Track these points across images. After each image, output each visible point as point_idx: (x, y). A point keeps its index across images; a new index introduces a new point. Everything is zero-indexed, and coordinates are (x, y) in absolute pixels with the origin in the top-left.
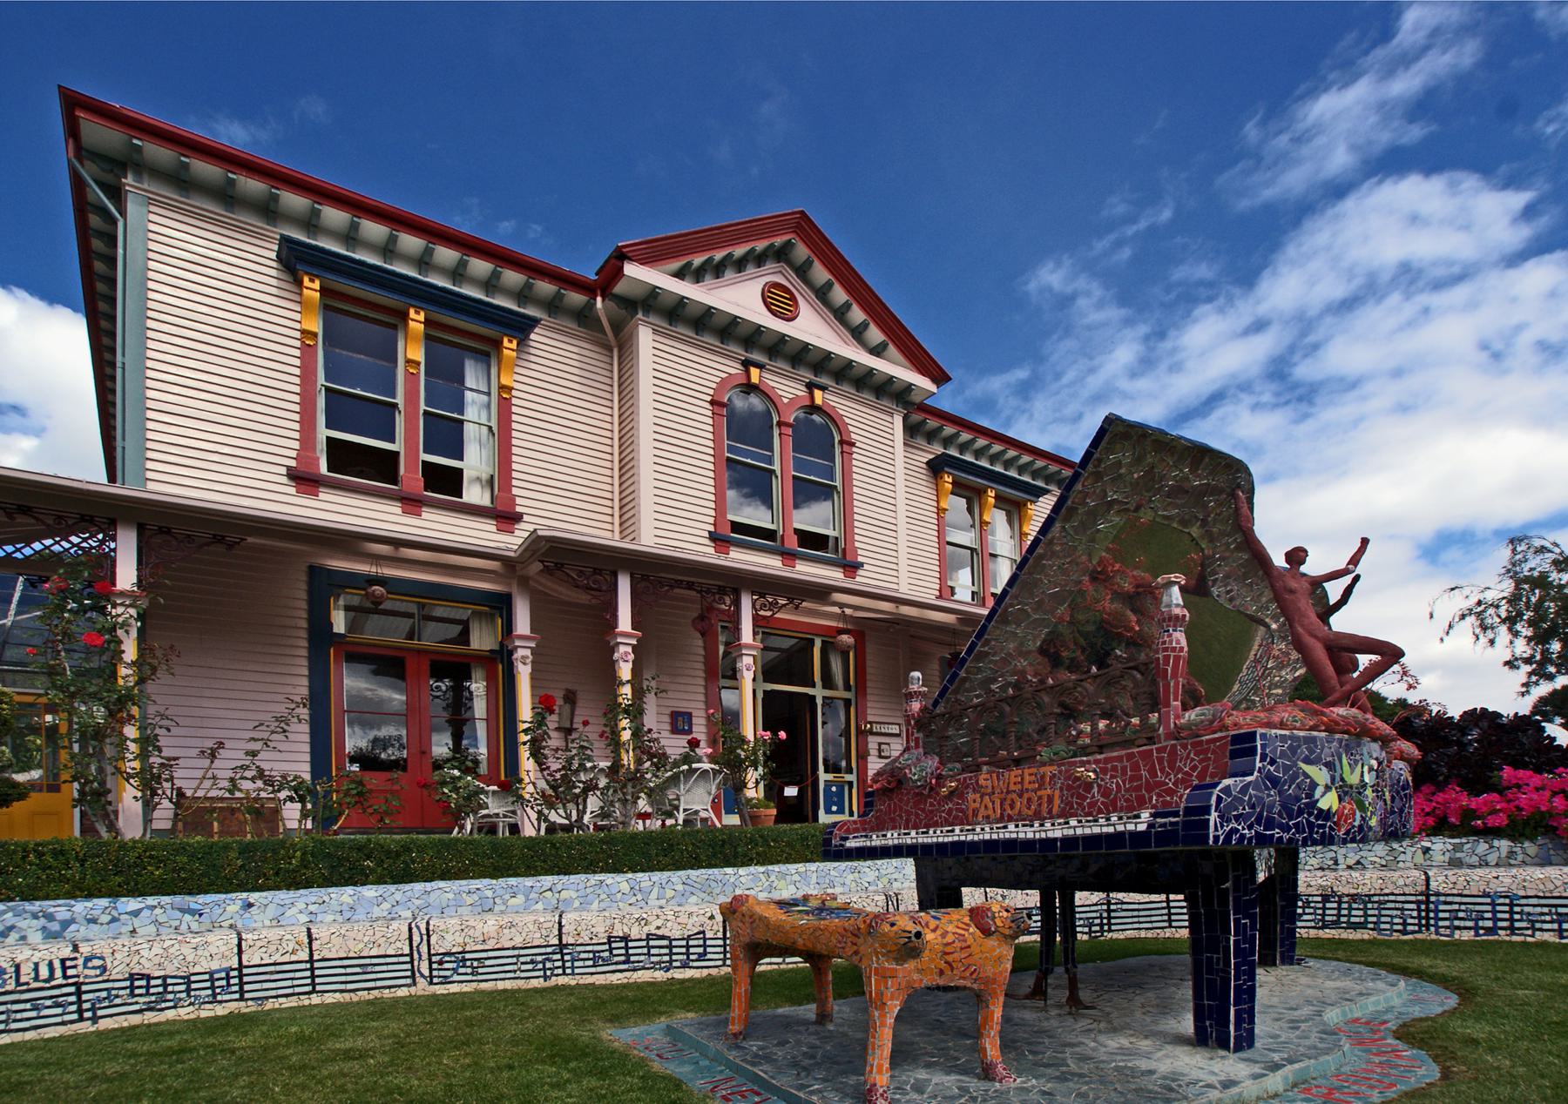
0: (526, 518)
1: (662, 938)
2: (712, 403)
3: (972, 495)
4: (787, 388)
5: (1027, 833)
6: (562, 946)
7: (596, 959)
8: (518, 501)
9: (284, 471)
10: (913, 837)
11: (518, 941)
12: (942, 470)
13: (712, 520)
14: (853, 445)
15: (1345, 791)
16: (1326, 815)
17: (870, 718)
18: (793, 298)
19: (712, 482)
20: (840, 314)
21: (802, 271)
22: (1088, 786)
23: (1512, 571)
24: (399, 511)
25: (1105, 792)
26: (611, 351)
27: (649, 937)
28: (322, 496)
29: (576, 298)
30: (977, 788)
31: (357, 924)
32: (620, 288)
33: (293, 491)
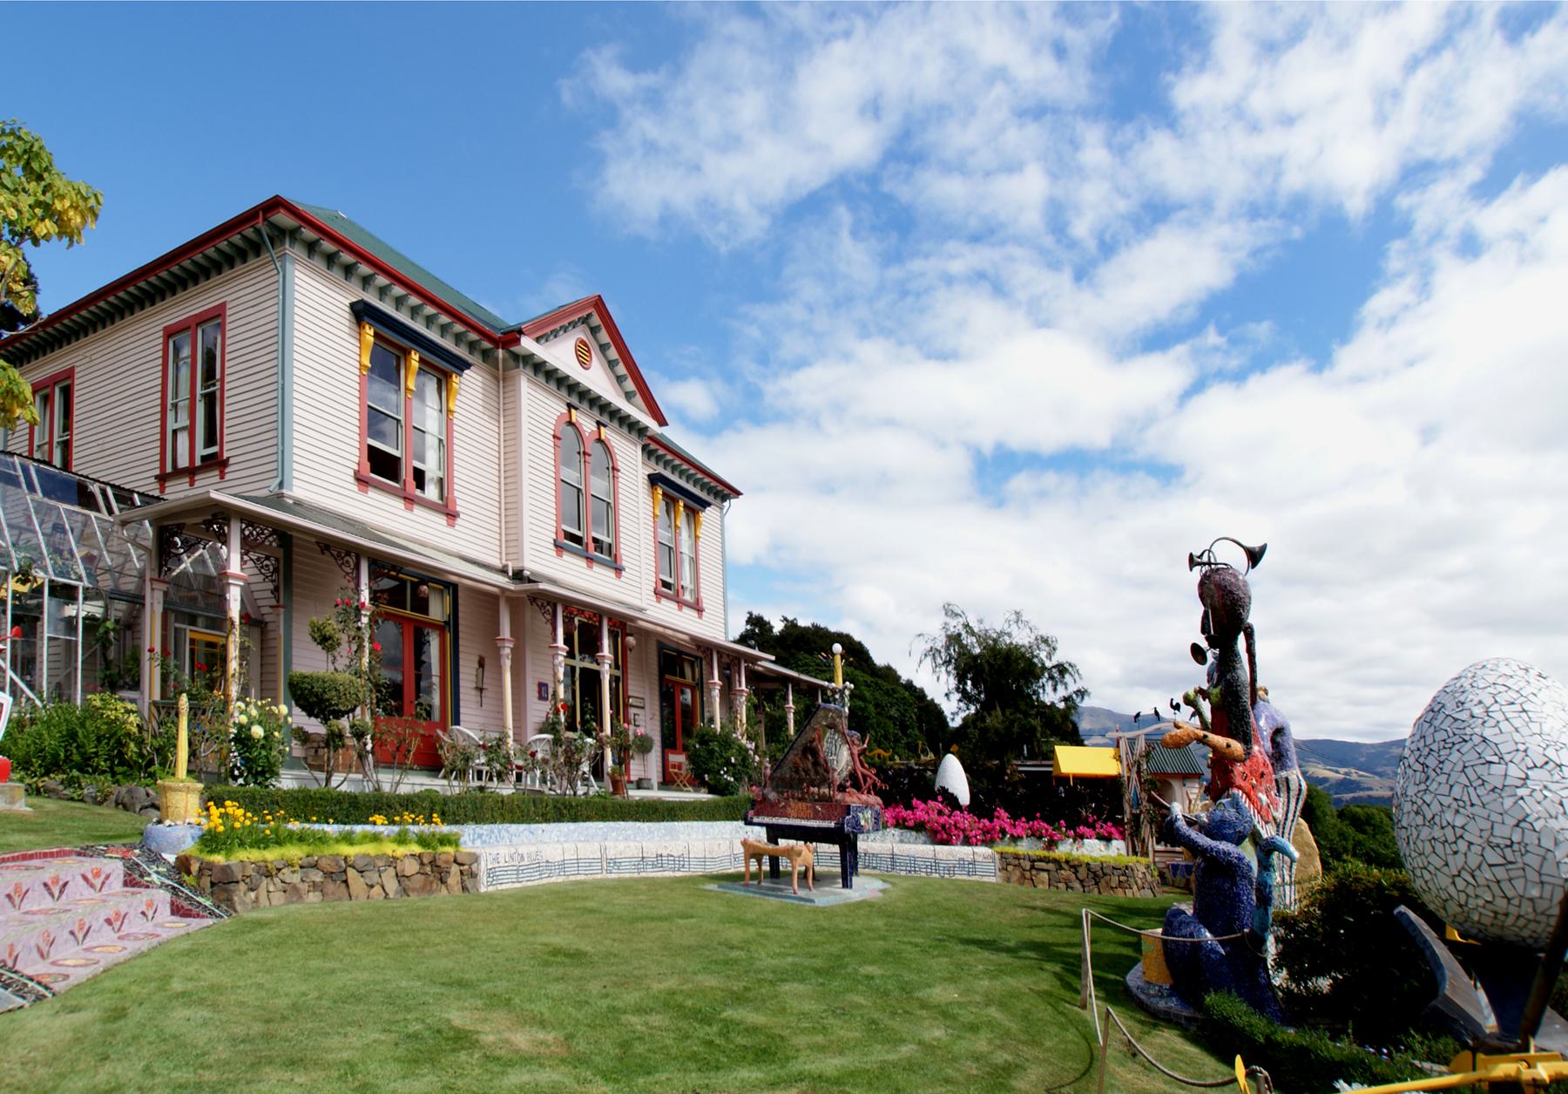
3: (670, 502)
4: (587, 423)
21: (594, 331)
29: (486, 345)
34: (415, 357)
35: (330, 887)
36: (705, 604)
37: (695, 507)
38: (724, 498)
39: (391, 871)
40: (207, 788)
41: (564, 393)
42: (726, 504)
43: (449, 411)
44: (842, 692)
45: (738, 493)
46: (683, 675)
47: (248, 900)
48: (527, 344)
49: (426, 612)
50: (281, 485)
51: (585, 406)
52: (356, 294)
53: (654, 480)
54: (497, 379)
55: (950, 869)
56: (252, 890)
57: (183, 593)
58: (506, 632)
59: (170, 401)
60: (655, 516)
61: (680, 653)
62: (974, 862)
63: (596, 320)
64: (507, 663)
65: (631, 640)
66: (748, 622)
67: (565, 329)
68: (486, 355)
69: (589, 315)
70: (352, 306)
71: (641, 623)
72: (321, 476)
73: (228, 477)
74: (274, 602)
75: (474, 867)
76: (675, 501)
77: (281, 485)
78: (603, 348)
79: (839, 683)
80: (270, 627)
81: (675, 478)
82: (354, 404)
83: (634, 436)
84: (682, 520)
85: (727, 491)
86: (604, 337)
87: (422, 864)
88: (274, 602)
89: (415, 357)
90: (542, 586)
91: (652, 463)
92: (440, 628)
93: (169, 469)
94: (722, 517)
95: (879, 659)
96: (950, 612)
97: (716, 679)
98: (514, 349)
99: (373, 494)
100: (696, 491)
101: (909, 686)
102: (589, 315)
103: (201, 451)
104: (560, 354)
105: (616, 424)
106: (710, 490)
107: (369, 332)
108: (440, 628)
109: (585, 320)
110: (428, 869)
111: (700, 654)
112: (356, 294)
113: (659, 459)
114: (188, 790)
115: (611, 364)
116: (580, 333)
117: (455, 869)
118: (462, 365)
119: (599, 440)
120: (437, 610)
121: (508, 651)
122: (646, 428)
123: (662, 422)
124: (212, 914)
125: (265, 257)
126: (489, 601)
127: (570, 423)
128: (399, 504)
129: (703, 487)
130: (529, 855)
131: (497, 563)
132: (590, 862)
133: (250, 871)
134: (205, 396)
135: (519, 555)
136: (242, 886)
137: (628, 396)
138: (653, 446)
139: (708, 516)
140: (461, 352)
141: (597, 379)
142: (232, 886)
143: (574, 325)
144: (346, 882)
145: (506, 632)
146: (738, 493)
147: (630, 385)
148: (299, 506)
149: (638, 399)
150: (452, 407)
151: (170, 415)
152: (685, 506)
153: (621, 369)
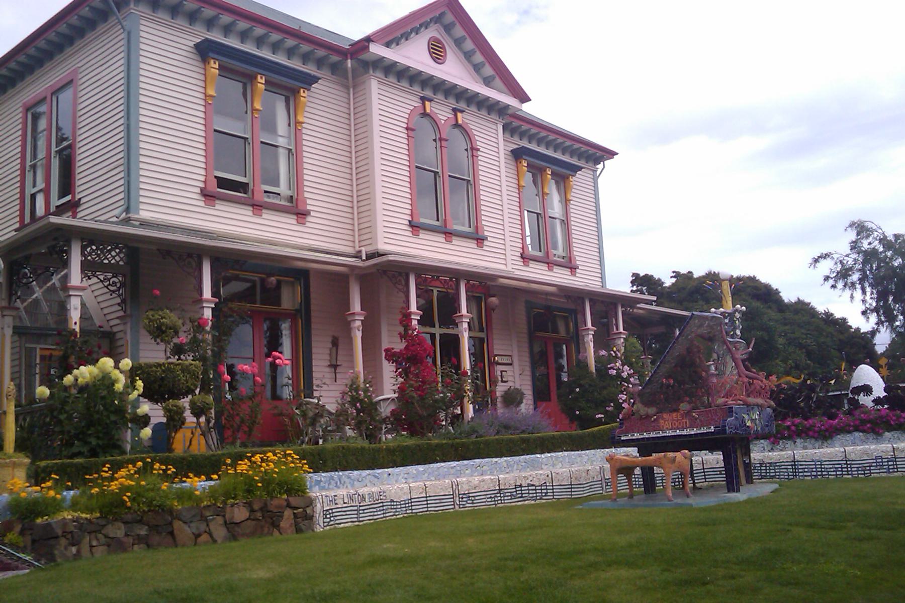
0: (312, 214)
1: (533, 485)
2: (407, 129)
3: (537, 172)
4: (442, 111)
5: (685, 433)
6: (500, 490)
7: (512, 496)
8: (309, 202)
9: (198, 190)
10: (637, 436)
11: (486, 488)
12: (521, 158)
13: (409, 212)
14: (478, 150)
15: (752, 420)
16: (748, 427)
17: (496, 353)
18: (443, 48)
19: (408, 185)
20: (477, 68)
21: (448, 28)
22: (696, 419)
23: (854, 246)
24: (250, 213)
25: (701, 421)
26: (349, 90)
27: (529, 485)
28: (217, 207)
29: (335, 58)
30: (663, 419)
31: (403, 484)
32: (364, 56)
33: (202, 204)
34: (261, 80)
35: (156, 539)
36: (579, 261)
37: (564, 175)
38: (598, 160)
39: (220, 520)
40: (32, 463)
41: (417, 88)
42: (600, 166)
43: (297, 123)
44: (731, 315)
45: (611, 154)
46: (555, 330)
47: (68, 553)
48: (376, 49)
49: (278, 303)
50: (127, 210)
51: (440, 97)
52: (200, 34)
53: (517, 155)
54: (347, 88)
55: (866, 469)
56: (73, 545)
57: (188, 504)
58: (356, 306)
59: (28, 163)
60: (519, 187)
61: (548, 308)
62: (895, 459)
63: (449, 18)
64: (358, 336)
65: (494, 300)
66: (633, 282)
67: (417, 31)
68: (336, 69)
69: (442, 15)
70: (197, 46)
71: (502, 280)
72: (172, 199)
73: (79, 215)
74: (121, 313)
75: (309, 511)
76: (542, 170)
77: (127, 210)
78: (458, 43)
79: (728, 307)
80: (118, 336)
81: (542, 150)
82: (199, 130)
83: (494, 116)
84: (552, 188)
85: (599, 153)
86: (459, 31)
87: (252, 511)
88: (121, 313)
89: (261, 80)
90: (391, 258)
91: (516, 139)
92: (292, 316)
93: (27, 220)
94: (595, 179)
95: (788, 296)
96: (862, 229)
97: (589, 325)
98: (364, 56)
99: (220, 205)
100: (566, 158)
101: (828, 318)
102: (442, 15)
103: (55, 202)
104: (414, 55)
105: (473, 108)
106: (580, 156)
107: (214, 65)
108: (292, 316)
109: (438, 20)
110: (259, 515)
111: (573, 307)
112: (200, 34)
113: (522, 135)
114: (15, 465)
115: (468, 56)
116: (433, 32)
117: (288, 513)
118: (309, 81)
119: (457, 125)
120: (289, 299)
121: (358, 323)
122: (507, 107)
123: (524, 98)
124: (30, 565)
125: (112, 20)
126: (338, 280)
127: (425, 114)
128: (247, 211)
129: (573, 153)
130: (371, 495)
131: (350, 250)
132: (440, 499)
133: (72, 527)
134: (60, 152)
135: (373, 239)
136: (63, 542)
137: (487, 82)
138: (516, 123)
139: (580, 180)
140: (310, 69)
141: (452, 70)
142: (52, 542)
143: (426, 25)
144: (172, 533)
145: (356, 306)
146: (611, 154)
147: (488, 71)
148: (144, 224)
149: (498, 82)
150: (300, 119)
151: (29, 177)
152: (553, 174)
153: (479, 58)
